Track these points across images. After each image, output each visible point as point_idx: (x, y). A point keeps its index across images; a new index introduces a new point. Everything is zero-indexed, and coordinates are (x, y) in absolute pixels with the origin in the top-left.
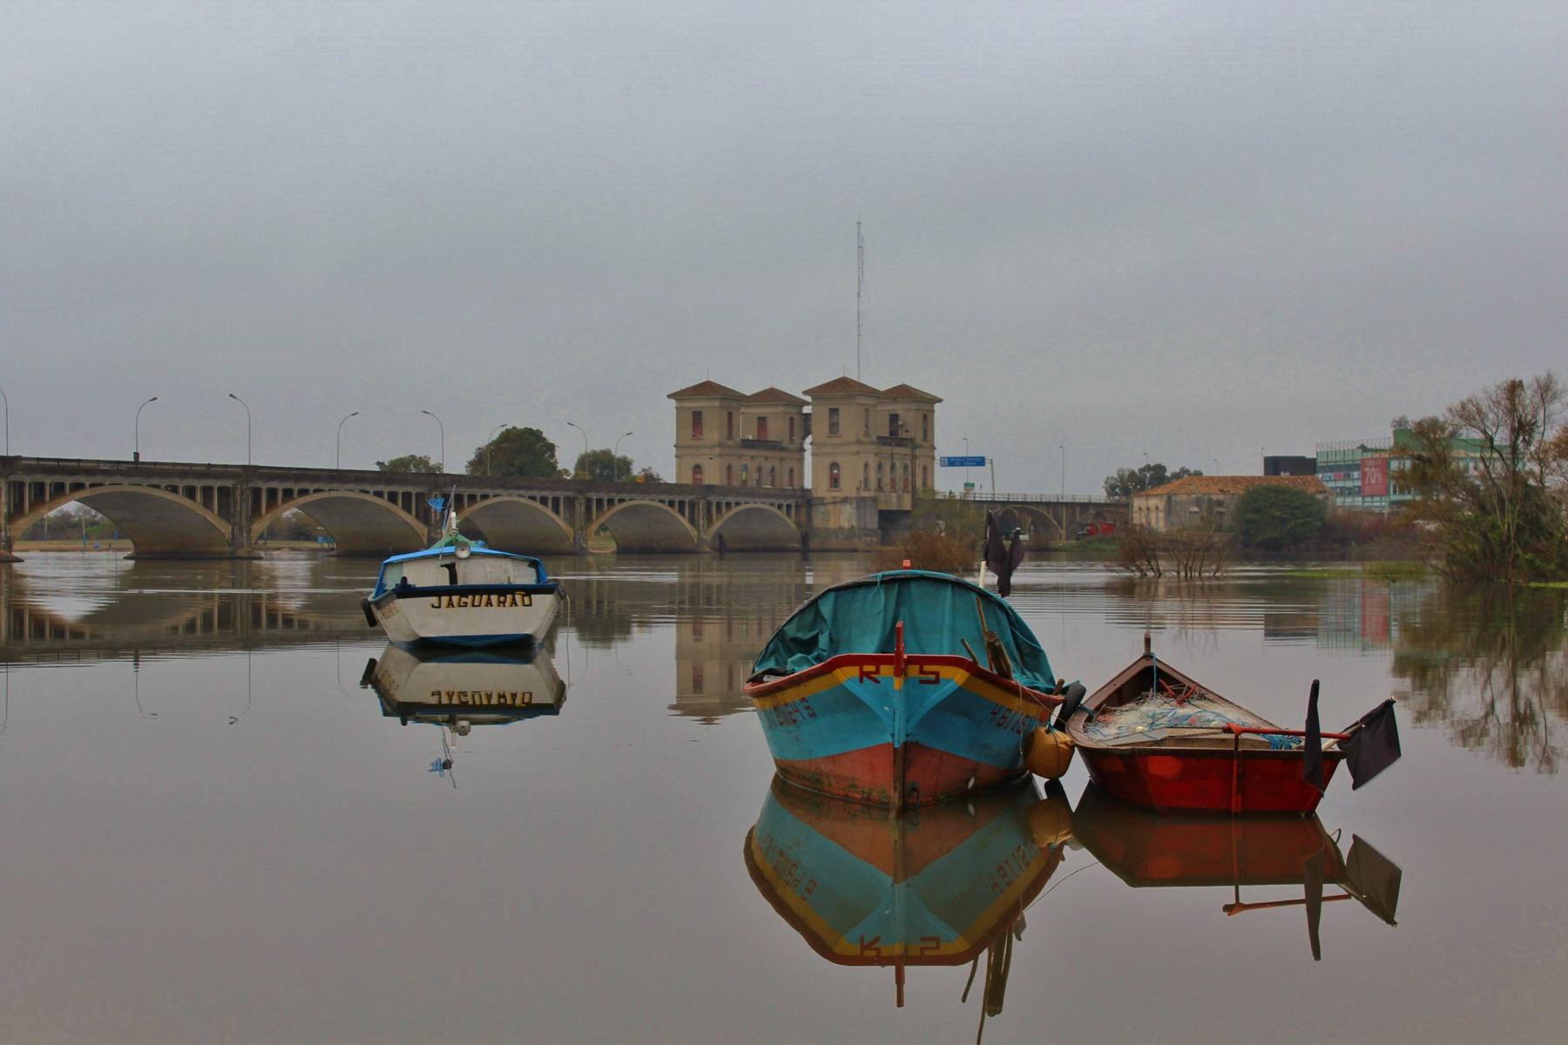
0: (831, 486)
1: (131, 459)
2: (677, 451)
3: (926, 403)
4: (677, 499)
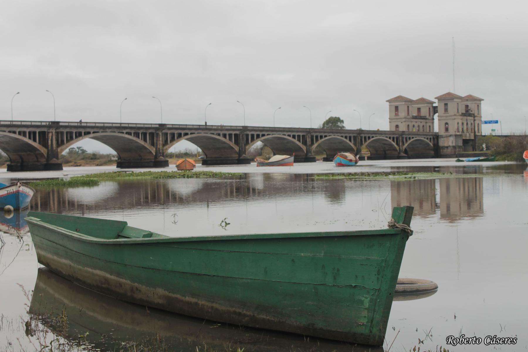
0: (446, 131)
1: (204, 124)
2: (438, 118)
3: (478, 101)
4: (392, 136)
